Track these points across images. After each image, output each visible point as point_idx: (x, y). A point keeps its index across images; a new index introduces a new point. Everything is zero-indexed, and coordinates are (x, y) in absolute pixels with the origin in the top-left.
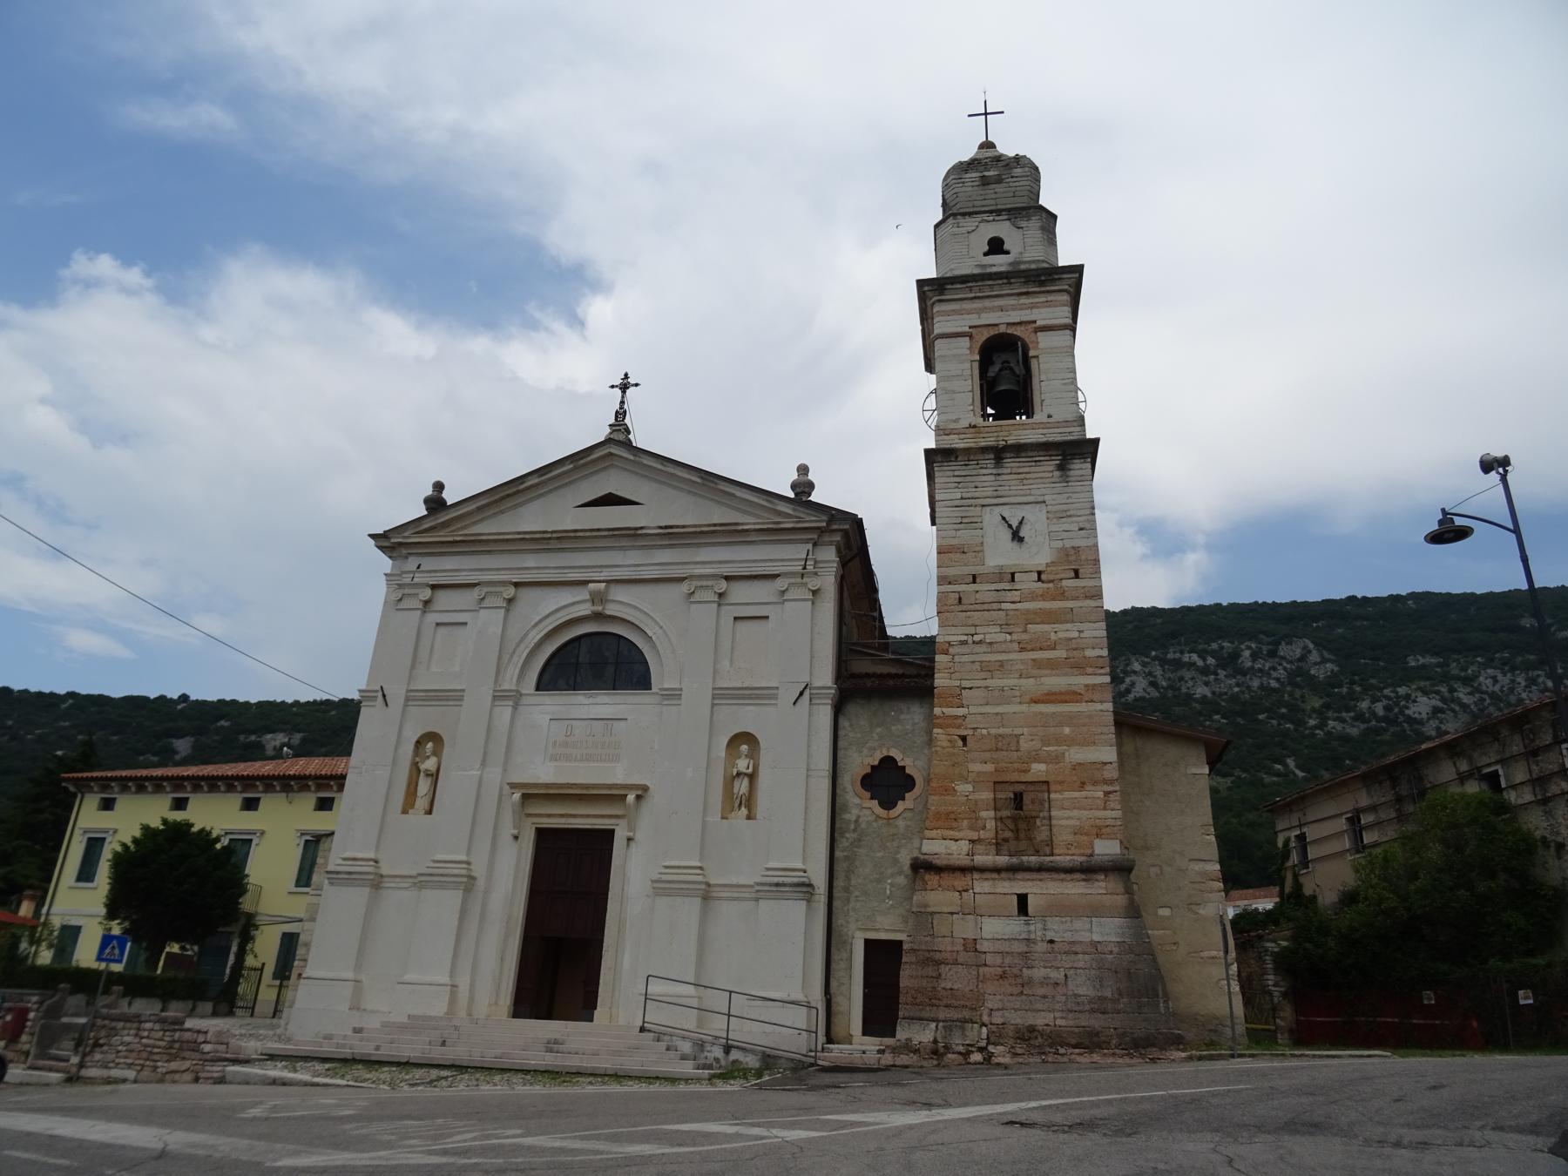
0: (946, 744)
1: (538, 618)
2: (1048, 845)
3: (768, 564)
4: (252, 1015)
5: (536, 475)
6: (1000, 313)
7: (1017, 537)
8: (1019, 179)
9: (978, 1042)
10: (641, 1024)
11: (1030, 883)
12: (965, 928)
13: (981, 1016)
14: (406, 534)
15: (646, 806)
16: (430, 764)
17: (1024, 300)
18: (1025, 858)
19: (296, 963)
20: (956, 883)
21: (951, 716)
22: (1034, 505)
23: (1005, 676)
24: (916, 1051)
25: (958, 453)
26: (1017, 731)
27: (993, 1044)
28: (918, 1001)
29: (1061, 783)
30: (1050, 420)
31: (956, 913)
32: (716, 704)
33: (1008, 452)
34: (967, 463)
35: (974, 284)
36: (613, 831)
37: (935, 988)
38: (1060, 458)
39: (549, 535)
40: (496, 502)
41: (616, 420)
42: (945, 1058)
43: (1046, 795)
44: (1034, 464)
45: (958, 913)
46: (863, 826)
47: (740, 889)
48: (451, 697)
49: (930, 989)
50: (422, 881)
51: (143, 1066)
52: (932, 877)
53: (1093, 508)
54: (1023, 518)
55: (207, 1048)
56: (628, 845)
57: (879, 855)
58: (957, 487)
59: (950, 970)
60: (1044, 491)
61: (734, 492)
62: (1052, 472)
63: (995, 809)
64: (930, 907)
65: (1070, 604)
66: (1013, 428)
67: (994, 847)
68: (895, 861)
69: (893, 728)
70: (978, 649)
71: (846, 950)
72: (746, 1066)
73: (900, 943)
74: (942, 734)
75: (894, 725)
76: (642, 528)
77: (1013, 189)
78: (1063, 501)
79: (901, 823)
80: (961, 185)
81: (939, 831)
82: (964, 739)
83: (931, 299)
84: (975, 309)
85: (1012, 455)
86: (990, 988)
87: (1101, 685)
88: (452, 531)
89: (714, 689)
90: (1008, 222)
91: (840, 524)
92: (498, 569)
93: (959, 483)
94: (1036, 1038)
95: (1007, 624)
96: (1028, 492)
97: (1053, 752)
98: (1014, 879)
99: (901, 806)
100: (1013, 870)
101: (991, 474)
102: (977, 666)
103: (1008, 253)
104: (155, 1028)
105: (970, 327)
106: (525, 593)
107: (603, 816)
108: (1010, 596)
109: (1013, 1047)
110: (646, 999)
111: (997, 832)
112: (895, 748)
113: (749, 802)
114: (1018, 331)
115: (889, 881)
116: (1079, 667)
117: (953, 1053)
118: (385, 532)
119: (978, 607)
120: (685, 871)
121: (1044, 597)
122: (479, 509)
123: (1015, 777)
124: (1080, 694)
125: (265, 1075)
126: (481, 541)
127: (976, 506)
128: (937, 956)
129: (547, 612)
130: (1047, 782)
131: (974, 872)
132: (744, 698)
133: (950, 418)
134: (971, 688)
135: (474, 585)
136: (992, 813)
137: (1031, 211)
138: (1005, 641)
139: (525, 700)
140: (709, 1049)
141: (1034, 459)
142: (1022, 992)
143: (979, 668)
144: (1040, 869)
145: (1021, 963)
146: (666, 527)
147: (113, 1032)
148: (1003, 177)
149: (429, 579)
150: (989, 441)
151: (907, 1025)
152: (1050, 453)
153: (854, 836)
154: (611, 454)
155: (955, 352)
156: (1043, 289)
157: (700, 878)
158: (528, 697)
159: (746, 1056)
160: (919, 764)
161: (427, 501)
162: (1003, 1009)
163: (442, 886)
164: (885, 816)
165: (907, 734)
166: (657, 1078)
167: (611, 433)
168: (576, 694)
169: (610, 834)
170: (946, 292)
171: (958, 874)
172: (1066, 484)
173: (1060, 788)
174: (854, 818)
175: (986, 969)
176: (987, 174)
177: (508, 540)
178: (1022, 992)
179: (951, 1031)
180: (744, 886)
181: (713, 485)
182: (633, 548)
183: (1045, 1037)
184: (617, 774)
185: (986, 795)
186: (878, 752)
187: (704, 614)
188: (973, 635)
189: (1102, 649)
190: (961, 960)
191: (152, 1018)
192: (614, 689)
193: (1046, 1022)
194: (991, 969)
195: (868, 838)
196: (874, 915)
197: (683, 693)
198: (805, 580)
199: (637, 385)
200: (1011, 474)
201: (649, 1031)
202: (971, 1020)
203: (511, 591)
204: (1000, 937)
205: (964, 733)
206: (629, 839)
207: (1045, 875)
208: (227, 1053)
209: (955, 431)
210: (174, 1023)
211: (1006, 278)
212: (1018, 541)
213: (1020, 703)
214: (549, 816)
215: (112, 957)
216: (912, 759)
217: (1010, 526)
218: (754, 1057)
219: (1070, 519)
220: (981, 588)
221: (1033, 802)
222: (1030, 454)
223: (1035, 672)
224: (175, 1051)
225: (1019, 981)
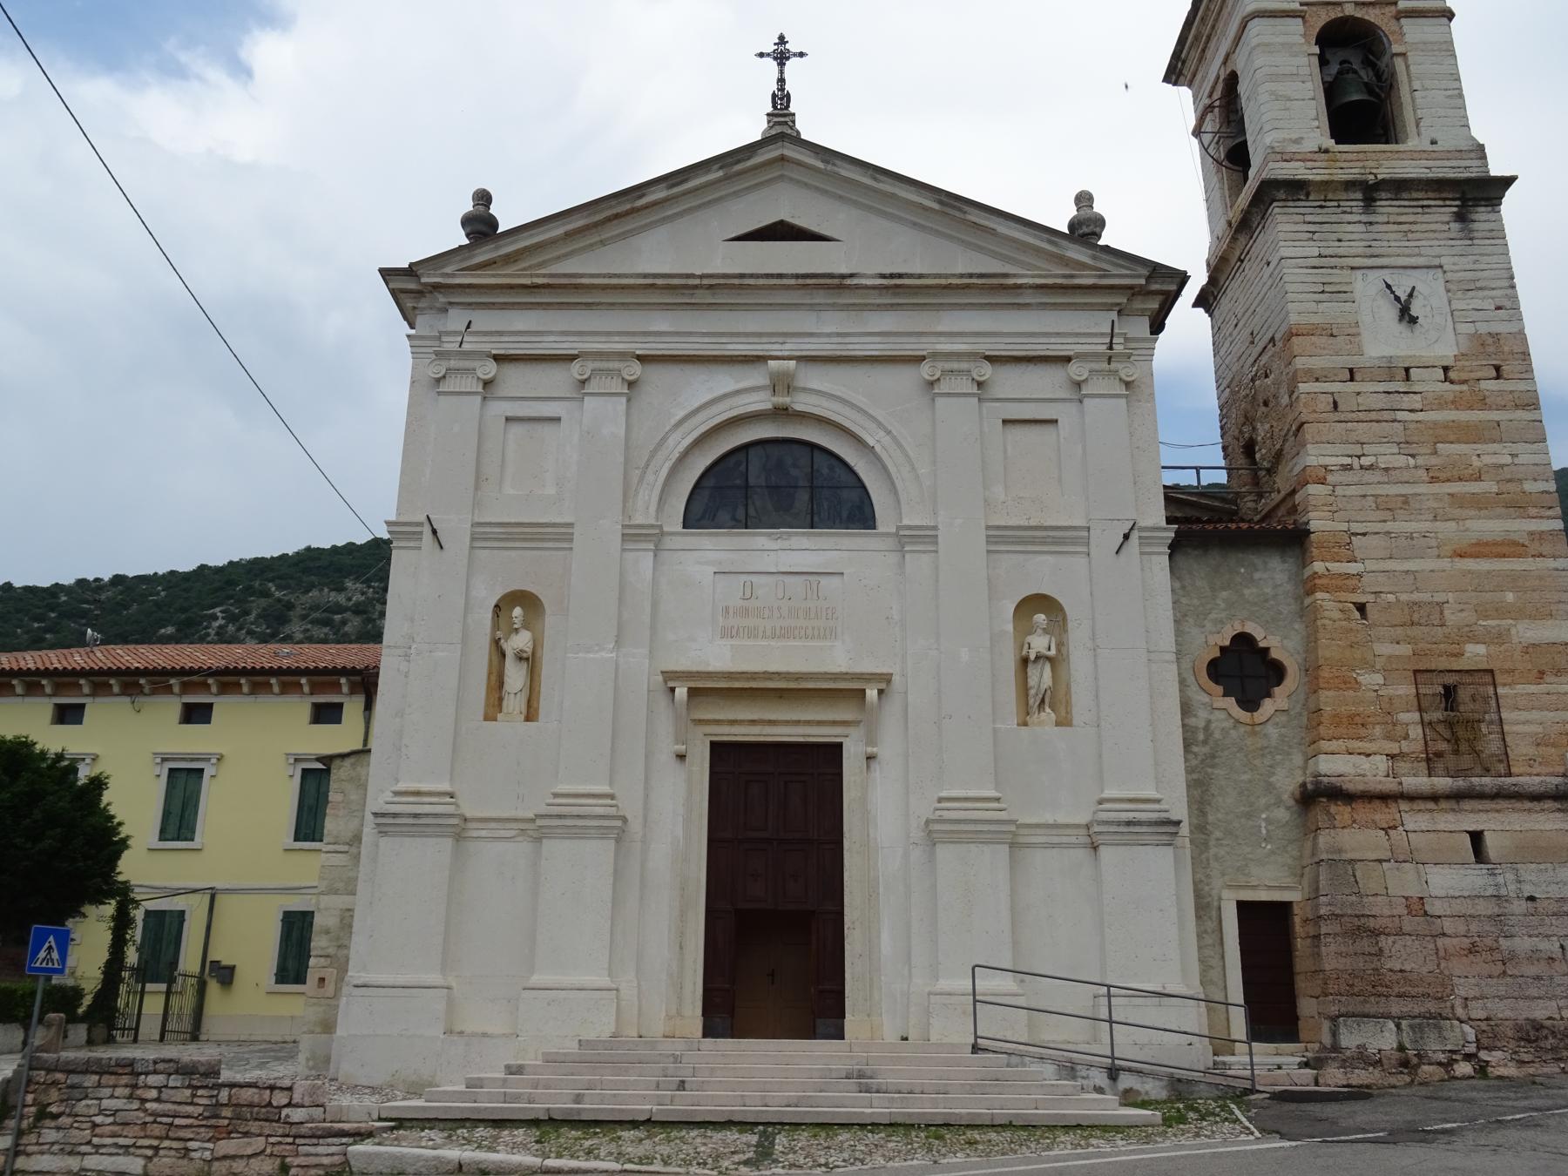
0: (1337, 615)
1: (681, 414)
2: (1500, 761)
3: (1053, 340)
4: (135, 1040)
5: (664, 185)
7: (1406, 314)
9: (1463, 1046)
11: (1484, 816)
12: (1404, 882)
13: (1453, 1007)
14: (448, 270)
15: (893, 707)
16: (520, 641)
18: (1475, 780)
19: (312, 962)
20: (1377, 817)
22: (1425, 270)
23: (1412, 517)
24: (1378, 1063)
26: (1440, 597)
27: (1486, 1048)
29: (1511, 671)
30: (1434, 147)
31: (1385, 861)
33: (1383, 190)
34: (1324, 204)
36: (838, 747)
37: (1377, 969)
38: (1458, 203)
39: (697, 282)
40: (596, 225)
41: (774, 107)
43: (1491, 690)
44: (1420, 210)
45: (1389, 861)
46: (1217, 735)
47: (1061, 831)
48: (560, 535)
50: (538, 829)
51: (156, 1149)
52: (1341, 809)
53: (1512, 278)
54: (1414, 288)
56: (868, 767)
57: (1245, 777)
59: (1394, 943)
60: (1437, 251)
61: (992, 225)
62: (1448, 223)
63: (1420, 710)
64: (1346, 852)
65: (1495, 415)
66: (1384, 156)
67: (1424, 764)
68: (1270, 788)
69: (1247, 592)
70: (1368, 476)
71: (1210, 918)
72: (1146, 1098)
76: (852, 276)
78: (1468, 267)
79: (1272, 730)
82: (1361, 608)
85: (1389, 196)
86: (1457, 967)
87: (1551, 533)
88: (524, 269)
89: (988, 528)
91: (1163, 283)
92: (609, 334)
93: (1314, 233)
94: (1546, 1038)
97: (1493, 627)
98: (1461, 811)
99: (1268, 707)
100: (1458, 796)
101: (1360, 222)
102: (1370, 501)
104: (171, 1084)
106: (660, 377)
107: (820, 723)
108: (1407, 401)
109: (1516, 1052)
110: (975, 1001)
111: (1426, 742)
112: (1253, 621)
113: (1055, 702)
116: (1518, 506)
117: (1429, 1064)
119: (1362, 416)
121: (1456, 404)
122: (569, 235)
123: (1443, 663)
124: (1523, 545)
125: (436, 1158)
127: (1342, 268)
128: (1372, 923)
129: (696, 405)
130: (1491, 671)
131: (1400, 801)
132: (1033, 543)
133: (1288, 137)
134: (1364, 534)
138: (1408, 467)
139: (668, 543)
140: (1084, 1073)
141: (1421, 203)
142: (1504, 972)
143: (1374, 505)
144: (1498, 795)
145: (1493, 929)
146: (892, 276)
147: (77, 1093)
150: (1352, 173)
152: (1444, 195)
153: (1206, 750)
155: (1281, 39)
157: (450, 809)
159: (1143, 1083)
160: (1289, 644)
161: (467, 221)
162: (1482, 997)
164: (1248, 721)
165: (1266, 601)
166: (1079, 1126)
167: (771, 128)
171: (1377, 803)
172: (1470, 242)
173: (1509, 680)
174: (1202, 724)
175: (1447, 941)
177: (623, 287)
178: (1504, 972)
179: (1422, 1031)
180: (1067, 826)
181: (957, 214)
183: (1559, 1036)
184: (837, 658)
185: (1406, 690)
188: (1359, 457)
189: (1547, 481)
190: (1406, 929)
191: (161, 1066)
192: (812, 528)
193: (1548, 1014)
194: (1455, 941)
195: (1226, 753)
196: (1246, 865)
198: (1113, 366)
199: (801, 55)
200: (1388, 223)
201: (986, 1050)
204: (1457, 894)
205: (1362, 599)
207: (1503, 804)
208: (324, 1121)
209: (1299, 157)
212: (1409, 322)
213: (1439, 556)
214: (733, 722)
215: (50, 965)
216: (1278, 638)
217: (1397, 299)
218: (1157, 1083)
219: (1481, 293)
221: (1473, 699)
222: (1415, 195)
223: (1457, 512)
224: (226, 1122)
225: (1497, 956)
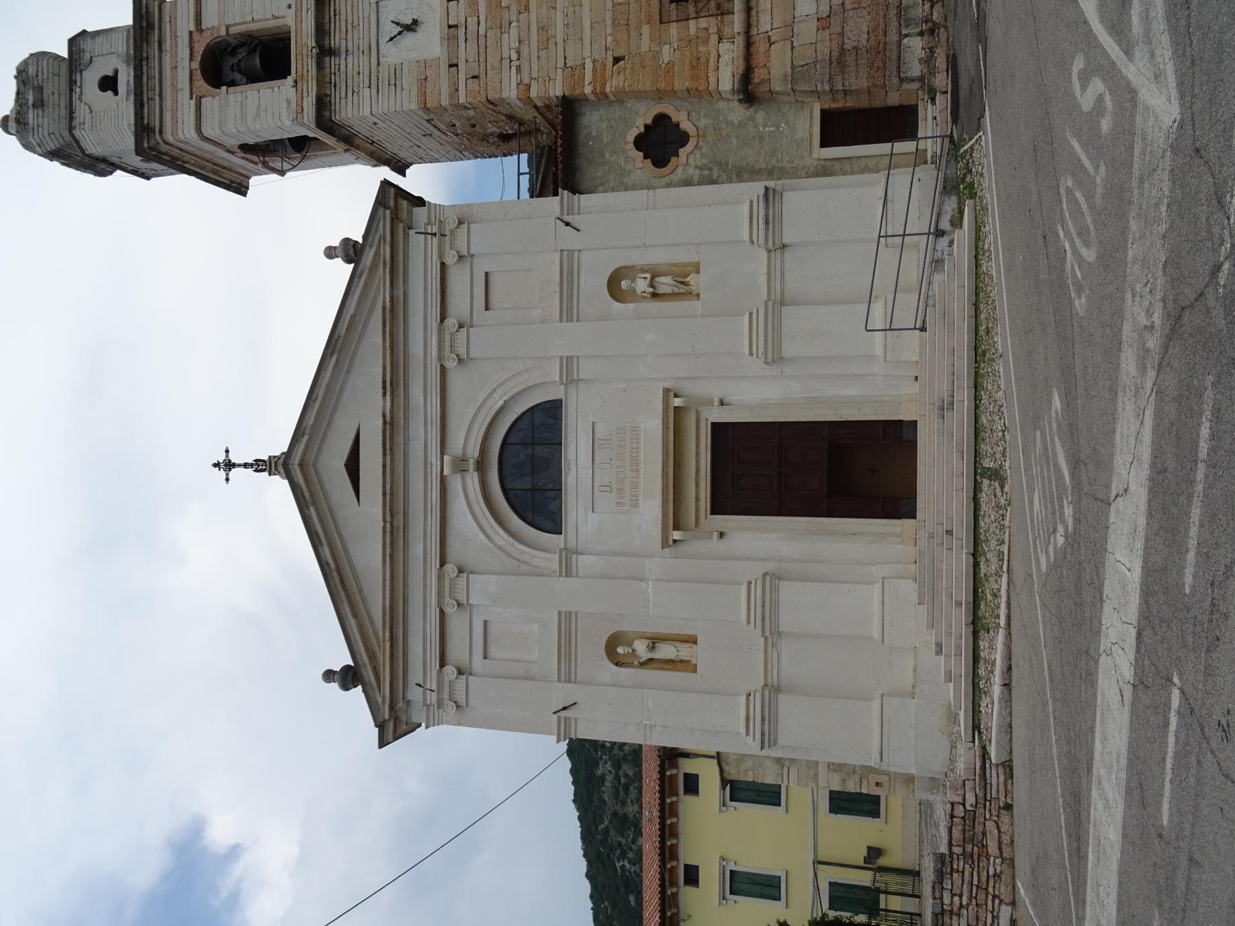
0: (622, 77)
1: (481, 536)
3: (429, 275)
4: (919, 915)
5: (320, 548)
6: (179, 69)
7: (412, 27)
8: (40, 69)
10: (917, 332)
12: (807, 32)
14: (380, 700)
15: (688, 387)
17: (167, 45)
19: (864, 791)
20: (762, 50)
21: (594, 75)
22: (380, 13)
25: (322, 93)
28: (881, 65)
31: (792, 44)
32: (577, 573)
34: (333, 84)
35: (145, 95)
39: (388, 525)
40: (348, 596)
41: (264, 470)
42: (937, 21)
44: (337, 17)
45: (792, 42)
49: (869, 56)
50: (772, 634)
51: (994, 897)
52: (756, 75)
54: (392, 22)
55: (970, 799)
56: (728, 404)
57: (735, 142)
58: (358, 93)
59: (849, 39)
61: (349, 317)
63: (687, 19)
67: (726, 17)
68: (741, 125)
69: (605, 141)
70: (525, 55)
72: (957, 211)
73: (824, 114)
74: (611, 82)
75: (602, 140)
76: (384, 416)
77: (50, 75)
80: (40, 129)
81: (710, 75)
82: (617, 60)
83: (158, 143)
84: (172, 95)
85: (327, 38)
88: (379, 646)
90: (84, 73)
91: (389, 198)
93: (353, 91)
95: (501, 27)
96: (366, 19)
99: (686, 126)
101: (346, 59)
103: (116, 72)
105: (191, 98)
106: (456, 551)
107: (698, 438)
110: (890, 329)
111: (710, 16)
114: (200, 49)
115: (761, 129)
117: (932, 14)
118: (376, 726)
119: (482, 59)
120: (754, 323)
122: (356, 615)
125: (1000, 702)
126: (392, 610)
127: (378, 72)
128: (835, 54)
129: (475, 525)
131: (751, 34)
132: (572, 289)
134: (565, 58)
135: (442, 613)
136: (692, 23)
137: (74, 49)
138: (518, 27)
139: (572, 544)
140: (940, 254)
141: (332, 16)
146: (384, 388)
148: (36, 85)
149: (433, 668)
151: (906, 66)
153: (716, 169)
154: (301, 465)
156: (156, 26)
158: (568, 540)
160: (642, 110)
161: (345, 687)
163: (775, 605)
164: (696, 139)
165: (612, 126)
168: (566, 483)
169: (717, 428)
170: (152, 125)
171: (752, 50)
174: (698, 171)
176: (31, 102)
177: (392, 577)
179: (909, 20)
181: (340, 342)
182: (406, 429)
184: (652, 426)
185: (674, 30)
186: (630, 153)
187: (481, 342)
190: (839, 30)
195: (718, 154)
196: (796, 141)
197: (565, 355)
198: (447, 233)
200: (346, 39)
201: (924, 322)
202: (898, 7)
203: (450, 670)
205: (610, 60)
206: (722, 403)
208: (975, 780)
210: (943, 863)
211: (141, 61)
213: (580, 6)
214: (697, 499)
217: (400, 33)
218: (946, 203)
220: (464, 58)
222: (327, 20)
224: (975, 848)
